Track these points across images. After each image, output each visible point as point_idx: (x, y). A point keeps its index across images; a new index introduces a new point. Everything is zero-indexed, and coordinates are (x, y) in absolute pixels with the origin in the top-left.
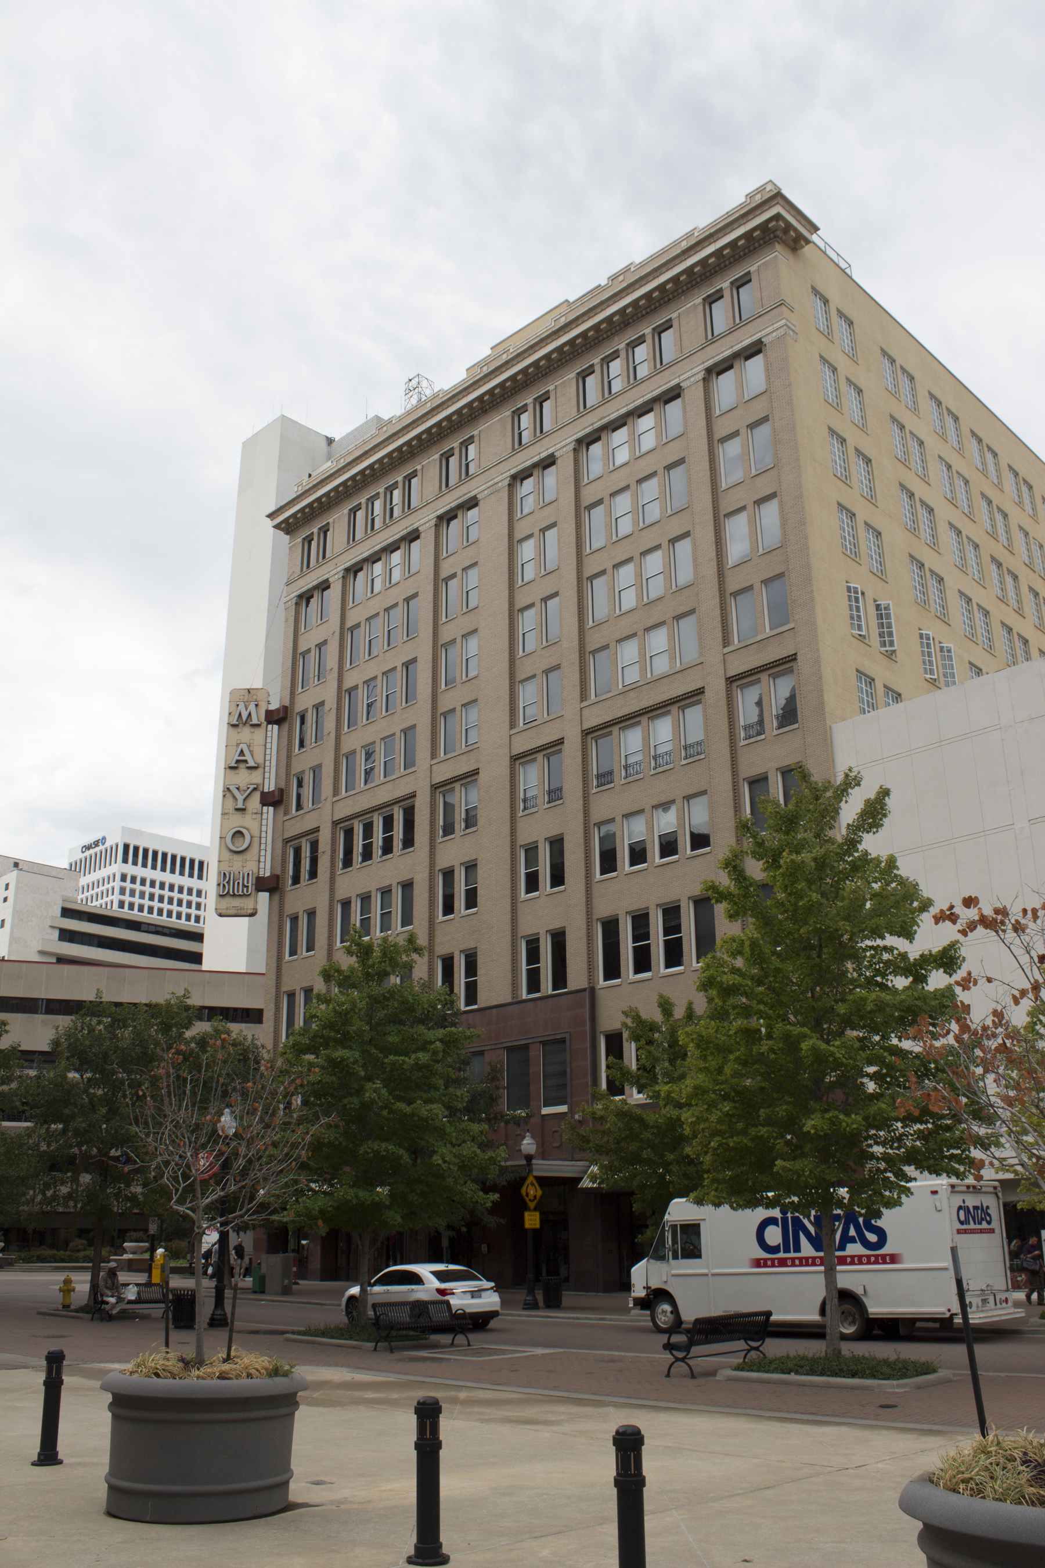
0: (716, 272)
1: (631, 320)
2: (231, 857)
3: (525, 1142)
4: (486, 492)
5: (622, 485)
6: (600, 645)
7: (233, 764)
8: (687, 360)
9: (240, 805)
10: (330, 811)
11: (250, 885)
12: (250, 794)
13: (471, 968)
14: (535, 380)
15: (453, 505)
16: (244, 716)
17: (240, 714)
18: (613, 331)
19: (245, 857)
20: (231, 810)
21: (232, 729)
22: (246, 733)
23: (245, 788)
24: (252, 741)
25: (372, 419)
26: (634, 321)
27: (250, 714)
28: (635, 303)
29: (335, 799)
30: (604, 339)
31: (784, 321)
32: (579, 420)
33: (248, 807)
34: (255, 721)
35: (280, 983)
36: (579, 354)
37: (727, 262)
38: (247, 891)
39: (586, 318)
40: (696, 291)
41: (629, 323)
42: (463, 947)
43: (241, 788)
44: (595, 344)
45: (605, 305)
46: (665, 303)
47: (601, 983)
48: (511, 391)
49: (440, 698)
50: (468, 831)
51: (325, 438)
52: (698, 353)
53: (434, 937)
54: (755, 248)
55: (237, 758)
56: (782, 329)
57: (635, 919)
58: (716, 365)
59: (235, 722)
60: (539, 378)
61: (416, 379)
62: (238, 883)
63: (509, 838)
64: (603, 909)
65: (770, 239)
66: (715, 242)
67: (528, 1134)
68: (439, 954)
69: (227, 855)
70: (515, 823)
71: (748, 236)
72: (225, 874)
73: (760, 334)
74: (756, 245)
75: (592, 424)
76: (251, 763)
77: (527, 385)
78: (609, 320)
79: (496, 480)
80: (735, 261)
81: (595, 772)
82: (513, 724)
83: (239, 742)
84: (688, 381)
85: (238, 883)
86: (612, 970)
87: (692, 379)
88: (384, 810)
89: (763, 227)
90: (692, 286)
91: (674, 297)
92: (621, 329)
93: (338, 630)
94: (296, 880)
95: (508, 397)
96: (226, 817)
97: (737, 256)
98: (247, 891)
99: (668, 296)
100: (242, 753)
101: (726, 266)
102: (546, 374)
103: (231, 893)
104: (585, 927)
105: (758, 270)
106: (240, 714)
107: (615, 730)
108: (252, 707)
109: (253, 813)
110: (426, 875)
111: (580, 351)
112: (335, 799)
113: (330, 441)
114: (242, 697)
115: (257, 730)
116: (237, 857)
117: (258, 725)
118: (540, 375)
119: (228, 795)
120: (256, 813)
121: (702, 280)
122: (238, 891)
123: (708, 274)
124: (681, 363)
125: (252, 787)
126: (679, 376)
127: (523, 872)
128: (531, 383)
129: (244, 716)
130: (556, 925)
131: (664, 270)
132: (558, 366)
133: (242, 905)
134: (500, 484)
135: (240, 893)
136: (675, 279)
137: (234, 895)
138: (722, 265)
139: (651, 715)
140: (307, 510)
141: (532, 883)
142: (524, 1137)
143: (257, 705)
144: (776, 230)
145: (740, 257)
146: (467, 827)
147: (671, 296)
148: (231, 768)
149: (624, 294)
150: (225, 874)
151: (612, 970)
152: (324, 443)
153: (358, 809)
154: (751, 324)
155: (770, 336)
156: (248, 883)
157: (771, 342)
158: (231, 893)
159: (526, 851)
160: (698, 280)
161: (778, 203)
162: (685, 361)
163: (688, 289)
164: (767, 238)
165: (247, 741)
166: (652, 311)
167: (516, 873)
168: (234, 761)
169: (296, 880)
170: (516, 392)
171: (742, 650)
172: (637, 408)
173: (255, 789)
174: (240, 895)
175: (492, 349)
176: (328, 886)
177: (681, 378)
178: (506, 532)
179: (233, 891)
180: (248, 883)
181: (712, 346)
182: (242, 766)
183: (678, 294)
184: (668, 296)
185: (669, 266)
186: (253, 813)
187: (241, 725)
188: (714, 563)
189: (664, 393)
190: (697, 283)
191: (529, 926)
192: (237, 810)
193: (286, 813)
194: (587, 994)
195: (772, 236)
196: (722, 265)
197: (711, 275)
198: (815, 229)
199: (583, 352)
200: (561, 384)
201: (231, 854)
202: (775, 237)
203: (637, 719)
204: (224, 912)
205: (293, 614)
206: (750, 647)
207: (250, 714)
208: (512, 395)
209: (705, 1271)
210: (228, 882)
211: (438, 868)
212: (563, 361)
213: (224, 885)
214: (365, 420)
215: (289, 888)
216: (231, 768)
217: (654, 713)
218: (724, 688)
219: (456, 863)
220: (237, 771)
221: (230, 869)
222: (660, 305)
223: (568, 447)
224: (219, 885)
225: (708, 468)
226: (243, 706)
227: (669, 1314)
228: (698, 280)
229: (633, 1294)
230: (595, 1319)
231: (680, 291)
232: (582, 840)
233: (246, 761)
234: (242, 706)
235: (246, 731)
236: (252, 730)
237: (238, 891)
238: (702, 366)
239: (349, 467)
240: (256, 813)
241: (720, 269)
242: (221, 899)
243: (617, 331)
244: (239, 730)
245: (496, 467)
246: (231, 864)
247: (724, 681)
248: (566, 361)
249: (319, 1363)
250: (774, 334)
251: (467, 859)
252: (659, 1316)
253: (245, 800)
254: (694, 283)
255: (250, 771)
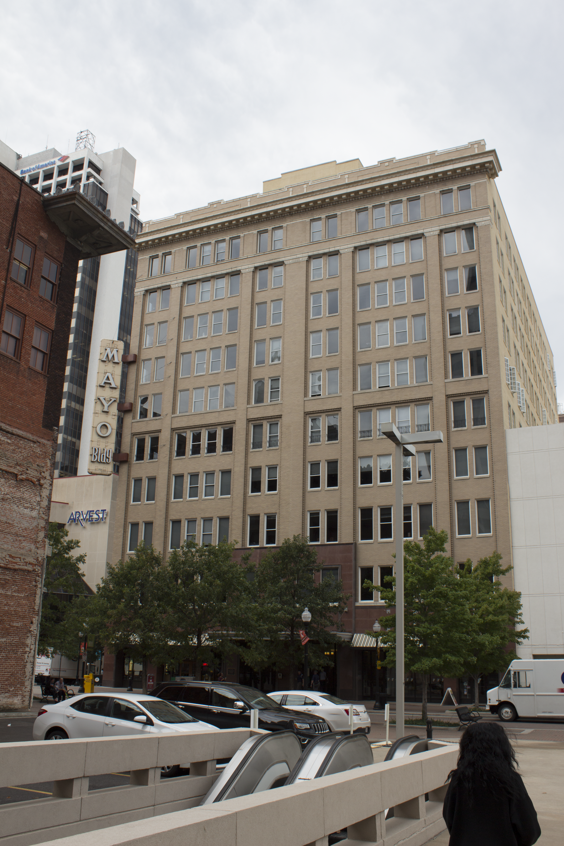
0: (449, 179)
1: (394, 190)
2: (99, 440)
3: (375, 625)
4: (291, 261)
5: (383, 279)
6: (366, 362)
7: (102, 384)
8: (429, 221)
9: (106, 409)
10: (170, 422)
11: (110, 457)
12: (111, 403)
13: (271, 522)
14: (327, 206)
15: (267, 263)
16: (110, 356)
17: (107, 355)
18: (382, 193)
19: (107, 440)
20: (100, 412)
21: (102, 364)
22: (110, 367)
23: (109, 399)
24: (113, 372)
25: (51, 150)
26: (396, 191)
27: (113, 356)
28: (400, 183)
29: (173, 416)
30: (375, 195)
31: (489, 217)
32: (357, 236)
33: (110, 411)
34: (116, 360)
35: (127, 517)
36: (358, 199)
37: (457, 176)
38: (109, 461)
39: (368, 182)
40: (436, 185)
41: (393, 191)
42: (267, 511)
43: (106, 400)
44: (369, 197)
45: (381, 179)
46: (416, 186)
47: (360, 541)
48: (311, 208)
49: (253, 371)
50: (271, 448)
51: (16, 154)
52: (436, 220)
53: (246, 504)
54: (474, 174)
55: (105, 381)
56: (488, 221)
57: (382, 510)
58: (446, 229)
59: (104, 359)
60: (330, 205)
61: (86, 133)
62: (103, 455)
63: (302, 457)
64: (363, 502)
65: (484, 172)
66: (453, 164)
67: (377, 621)
68: (249, 513)
69: (96, 438)
70: (306, 449)
71: (473, 167)
72: (95, 449)
73: (474, 220)
74: (475, 172)
75: (366, 241)
76: (113, 385)
77: (322, 207)
78: (382, 187)
79: (298, 256)
80: (461, 176)
81: (359, 430)
82: (306, 395)
83: (106, 371)
84: (429, 233)
85: (103, 455)
86: (367, 533)
87: (432, 233)
88: (210, 427)
89: (482, 165)
90: (434, 182)
91: (422, 185)
92: (387, 193)
93: (177, 317)
94: (140, 456)
95: (309, 210)
96: (97, 415)
97: (463, 175)
98: (109, 461)
99: (419, 183)
100: (108, 378)
101: (455, 178)
102: (335, 204)
103: (99, 461)
104: (352, 510)
105: (475, 186)
106: (107, 355)
107: (374, 409)
108: (115, 352)
109: (112, 415)
110: (243, 468)
111: (359, 198)
112: (173, 416)
113: (19, 157)
114: (108, 345)
115: (116, 366)
116: (102, 440)
117: (118, 363)
118: (331, 204)
119: (99, 402)
120: (115, 415)
121: (440, 181)
122: (103, 460)
123: (445, 179)
124: (424, 222)
125: (113, 400)
126: (423, 229)
127: (309, 476)
128: (325, 207)
129: (110, 356)
130: (332, 507)
131: (421, 170)
132: (344, 202)
133: (104, 469)
134: (301, 259)
135: (104, 461)
136: (426, 177)
137: (101, 462)
138: (454, 177)
139: (397, 405)
140: (156, 241)
141: (315, 482)
142: (374, 623)
143: (117, 351)
144: (488, 168)
145: (465, 176)
146: (270, 446)
147: (420, 184)
148: (101, 386)
149: (394, 176)
150: (95, 449)
151: (367, 533)
152: (15, 158)
153: (191, 424)
154: (469, 213)
155: (480, 223)
156: (109, 456)
157: (481, 226)
158: (99, 461)
159: (311, 465)
160: (438, 180)
161: (493, 155)
162: (428, 222)
163: (431, 183)
164: (482, 171)
165: (111, 371)
166: (407, 188)
167: (305, 476)
168: (103, 382)
169: (140, 456)
170: (314, 209)
171: (456, 382)
172: (395, 239)
173: (115, 401)
174: (104, 463)
175: (282, 174)
176: (167, 465)
177: (425, 230)
178: (305, 287)
179: (100, 460)
180: (109, 456)
181: (444, 218)
182: (107, 386)
183: (425, 184)
184: (419, 183)
185: (424, 169)
186: (112, 415)
187: (107, 361)
188: (441, 334)
189: (412, 236)
190: (437, 182)
191: (312, 506)
192: (103, 412)
193: (134, 418)
194: (353, 546)
195: (485, 170)
196: (454, 177)
197: (446, 180)
198: (501, 170)
199: (361, 199)
200: (345, 212)
201: (99, 437)
202: (486, 171)
203: (389, 406)
204: (94, 472)
205: (142, 300)
206: (460, 382)
207: (113, 356)
208: (311, 210)
209: (533, 694)
210: (97, 455)
211: (249, 466)
212: (348, 200)
213: (95, 456)
214: (45, 149)
215: (134, 462)
216: (101, 386)
217: (399, 405)
218: (445, 400)
219: (263, 465)
220: (104, 389)
221: (98, 446)
222: (413, 187)
223: (349, 249)
224: (91, 455)
225: (440, 283)
226: (110, 351)
227: (509, 713)
228: (438, 180)
229: (488, 703)
230: (434, 715)
231: (427, 183)
232: (352, 465)
233: (110, 384)
234: (108, 350)
235: (111, 365)
236: (114, 365)
237: (103, 460)
238: (438, 227)
239: (192, 224)
240: (115, 415)
241: (452, 178)
242: (92, 464)
243: (384, 193)
244: (106, 364)
245: (298, 249)
246: (99, 444)
247: (445, 396)
248: (350, 201)
249: (453, 737)
250: (483, 223)
251: (271, 464)
252: (504, 714)
253: (109, 406)
254: (435, 181)
255: (112, 390)
